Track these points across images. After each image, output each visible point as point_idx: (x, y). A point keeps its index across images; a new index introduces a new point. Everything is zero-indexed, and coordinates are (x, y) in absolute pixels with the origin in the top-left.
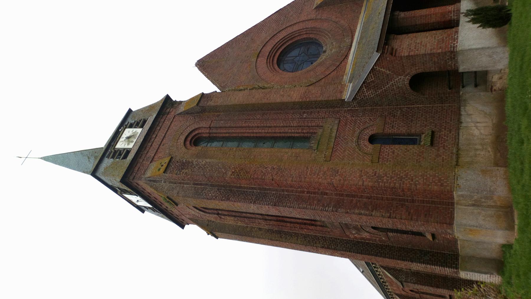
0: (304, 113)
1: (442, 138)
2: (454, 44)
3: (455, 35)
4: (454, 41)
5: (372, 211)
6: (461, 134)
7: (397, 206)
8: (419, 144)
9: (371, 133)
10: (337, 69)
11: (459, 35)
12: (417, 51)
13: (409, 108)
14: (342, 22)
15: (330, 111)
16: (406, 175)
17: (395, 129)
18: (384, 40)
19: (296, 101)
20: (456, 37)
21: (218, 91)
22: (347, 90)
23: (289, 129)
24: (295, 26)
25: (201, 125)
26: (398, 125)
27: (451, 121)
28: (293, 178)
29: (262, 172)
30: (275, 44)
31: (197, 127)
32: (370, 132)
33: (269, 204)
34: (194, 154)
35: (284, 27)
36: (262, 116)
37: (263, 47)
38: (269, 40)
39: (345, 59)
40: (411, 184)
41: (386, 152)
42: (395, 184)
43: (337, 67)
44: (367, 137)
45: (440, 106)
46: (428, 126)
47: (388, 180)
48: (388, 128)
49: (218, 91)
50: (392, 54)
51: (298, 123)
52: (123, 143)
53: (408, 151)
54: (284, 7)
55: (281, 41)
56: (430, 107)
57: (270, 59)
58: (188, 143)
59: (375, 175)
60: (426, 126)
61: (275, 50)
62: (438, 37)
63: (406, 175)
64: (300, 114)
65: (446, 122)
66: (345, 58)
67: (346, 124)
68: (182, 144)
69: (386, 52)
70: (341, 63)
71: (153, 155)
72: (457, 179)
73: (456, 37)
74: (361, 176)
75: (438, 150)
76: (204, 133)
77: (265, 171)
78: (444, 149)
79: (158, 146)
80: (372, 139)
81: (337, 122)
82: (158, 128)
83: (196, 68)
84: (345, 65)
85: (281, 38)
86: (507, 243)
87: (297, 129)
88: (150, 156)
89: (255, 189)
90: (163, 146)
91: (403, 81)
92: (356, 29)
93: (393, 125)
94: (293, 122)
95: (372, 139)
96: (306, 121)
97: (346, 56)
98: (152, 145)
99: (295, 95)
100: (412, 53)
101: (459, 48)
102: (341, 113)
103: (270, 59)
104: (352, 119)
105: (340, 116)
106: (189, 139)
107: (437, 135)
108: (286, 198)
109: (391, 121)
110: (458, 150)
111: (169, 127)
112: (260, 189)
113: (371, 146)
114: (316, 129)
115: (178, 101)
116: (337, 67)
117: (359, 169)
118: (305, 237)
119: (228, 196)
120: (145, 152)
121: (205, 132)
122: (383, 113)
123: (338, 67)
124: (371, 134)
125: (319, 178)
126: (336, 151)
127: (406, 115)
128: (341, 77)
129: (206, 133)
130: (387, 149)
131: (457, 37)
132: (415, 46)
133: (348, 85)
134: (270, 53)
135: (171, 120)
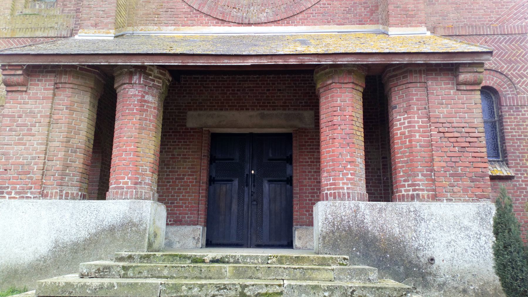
2: (9, 193)
3: (32, 193)
4: (16, 193)
10: (195, 11)
11: (32, 200)
12: (11, 130)
18: (28, 64)
20: (29, 195)
22: (96, 35)
43: (198, 11)
66: (218, 19)
70: (207, 15)
86: (64, 276)
97: (222, 20)
116: (198, 11)
118: (349, 67)
123: (198, 12)
128: (172, 22)
132: (25, 125)
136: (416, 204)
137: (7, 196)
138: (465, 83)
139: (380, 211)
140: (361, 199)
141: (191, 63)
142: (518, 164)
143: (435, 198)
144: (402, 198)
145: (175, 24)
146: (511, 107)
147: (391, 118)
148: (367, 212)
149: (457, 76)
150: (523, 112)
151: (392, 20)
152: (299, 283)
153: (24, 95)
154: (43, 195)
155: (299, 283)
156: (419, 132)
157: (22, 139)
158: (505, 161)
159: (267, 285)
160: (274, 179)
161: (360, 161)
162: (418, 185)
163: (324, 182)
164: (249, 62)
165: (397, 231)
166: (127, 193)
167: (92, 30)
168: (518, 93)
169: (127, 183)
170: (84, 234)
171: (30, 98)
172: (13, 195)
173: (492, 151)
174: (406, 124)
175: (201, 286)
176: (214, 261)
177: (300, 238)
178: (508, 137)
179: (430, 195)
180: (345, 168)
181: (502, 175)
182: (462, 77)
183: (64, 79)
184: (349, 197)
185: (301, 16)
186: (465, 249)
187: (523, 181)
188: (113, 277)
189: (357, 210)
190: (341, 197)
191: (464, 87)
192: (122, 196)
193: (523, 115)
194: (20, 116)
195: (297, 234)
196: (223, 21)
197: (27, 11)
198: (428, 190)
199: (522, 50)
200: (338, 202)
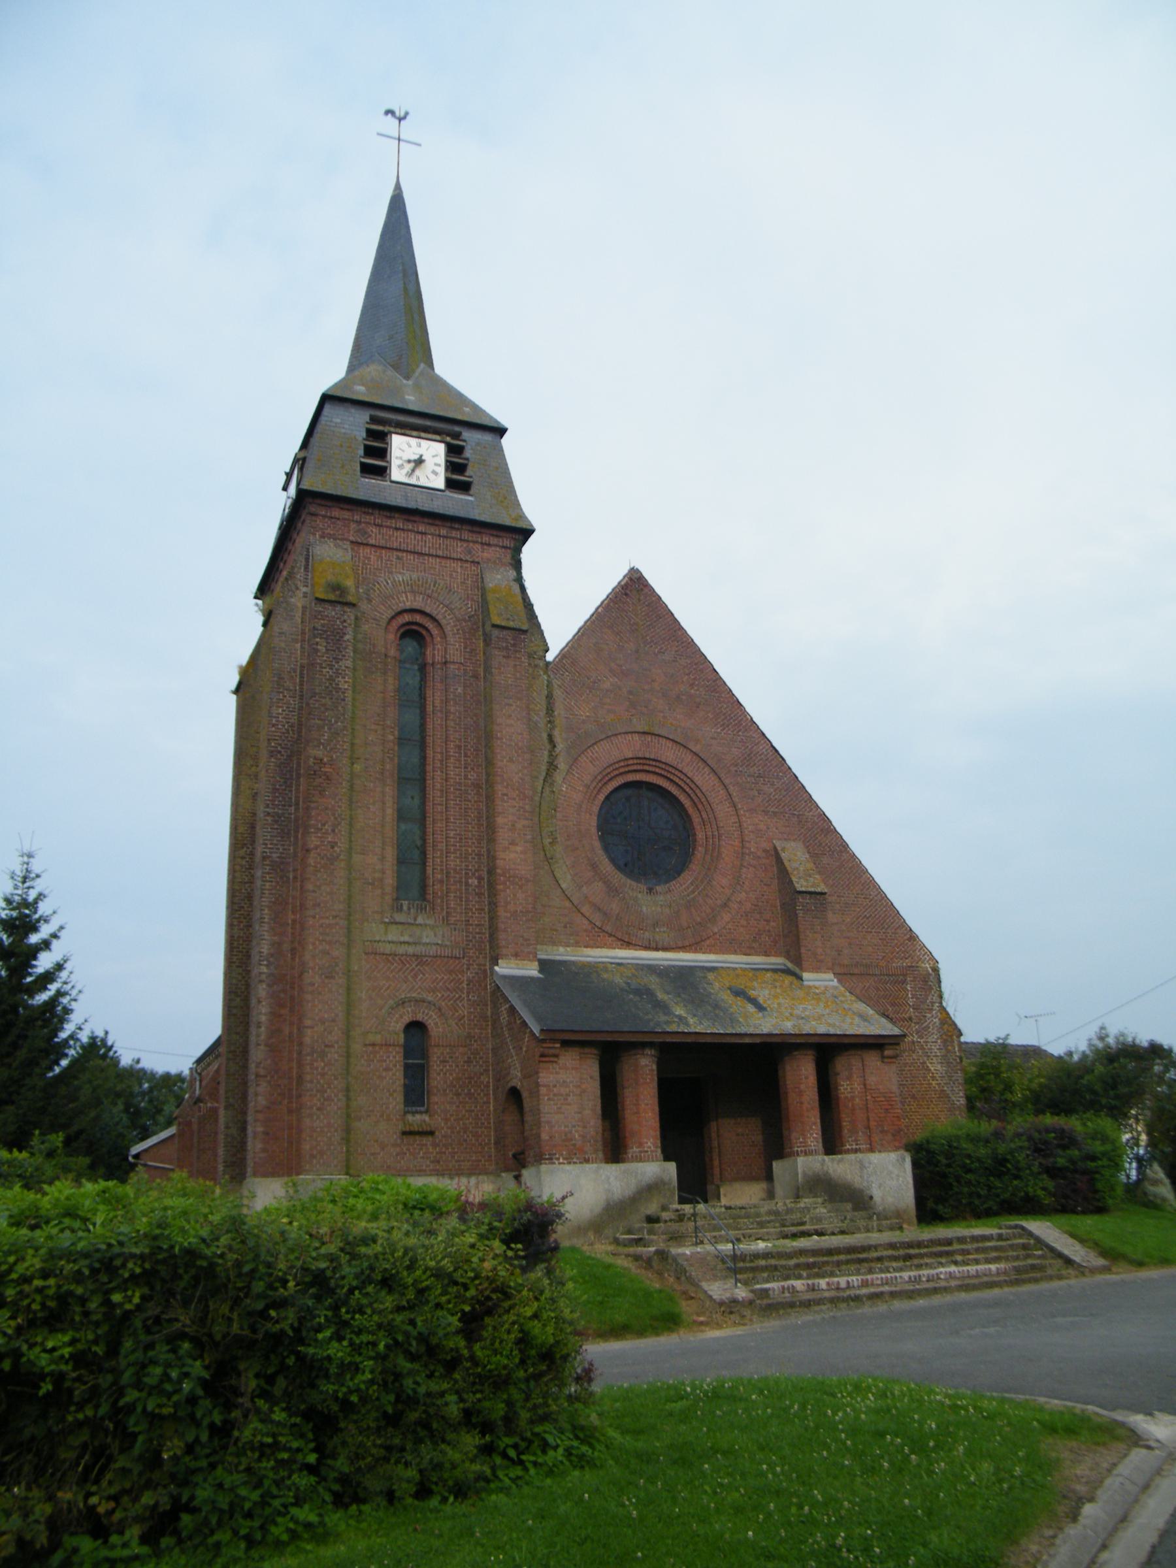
0: (480, 879)
1: (421, 1149)
3: (578, 1158)
4: (564, 1159)
5: (266, 1045)
7: (279, 1086)
8: (406, 1113)
9: (430, 1024)
12: (549, 1099)
13: (487, 1086)
14: (726, 917)
15: (484, 934)
16: (329, 1099)
17: (438, 1066)
19: (498, 861)
20: (575, 1160)
23: (442, 850)
25: (451, 639)
26: (447, 1070)
27: (457, 1161)
28: (314, 891)
29: (324, 825)
30: (680, 767)
31: (448, 629)
32: (432, 1020)
33: (266, 844)
34: (374, 646)
35: (727, 782)
36: (473, 784)
37: (673, 740)
38: (692, 751)
39: (619, 943)
40: (311, 1108)
42: (311, 1082)
45: (490, 1140)
46: (446, 1124)
47: (317, 1068)
48: (442, 1053)
49: (550, 657)
50: (542, 1055)
51: (455, 870)
53: (391, 1095)
54: (790, 768)
55: (688, 781)
56: (489, 1123)
58: (407, 618)
59: (326, 1046)
60: (446, 1120)
61: (663, 772)
62: (576, 1131)
63: (329, 1099)
64: (476, 871)
65: (455, 1153)
67: (451, 972)
68: (401, 606)
69: (545, 1045)
70: (610, 935)
71: (372, 542)
74: (322, 1021)
75: (395, 1145)
76: (434, 649)
77: (327, 830)
78: (397, 1155)
79: (395, 545)
80: (416, 1028)
81: (456, 953)
82: (443, 532)
83: (625, 571)
84: (605, 944)
85: (696, 779)
87: (442, 870)
88: (370, 536)
89: (297, 809)
90: (398, 558)
91: (516, 1079)
92: (704, 953)
93: (448, 1062)
94: (457, 857)
95: (416, 1028)
96: (461, 886)
98: (397, 529)
99: (512, 855)
100: (543, 1090)
101: (544, 1168)
102: (478, 957)
104: (463, 982)
105: (470, 957)
106: (418, 618)
107: (427, 1140)
108: (281, 878)
109: (457, 1058)
111: (446, 558)
112: (296, 820)
113: (400, 1026)
114: (442, 909)
115: (522, 555)
117: (337, 1015)
119: (280, 752)
120: (378, 521)
121: (434, 653)
122: (475, 1041)
124: (427, 1023)
125: (314, 944)
126: (388, 961)
127: (470, 1082)
129: (434, 655)
130: (395, 1057)
131: (575, 1163)
134: (654, 760)
135: (468, 558)
136: (860, 1155)
144: (848, 1152)
147: (1029, 1217)
149: (882, 1052)
151: (805, 964)
153: (554, 1065)
157: (560, 1108)
167: (513, 962)
171: (560, 1068)
172: (561, 1161)
177: (725, 1195)
179: (814, 1137)
180: (811, 1129)
182: (887, 1053)
183: (587, 1050)
186: (692, 1298)
194: (555, 1086)
196: (628, 944)
200: (810, 1158)
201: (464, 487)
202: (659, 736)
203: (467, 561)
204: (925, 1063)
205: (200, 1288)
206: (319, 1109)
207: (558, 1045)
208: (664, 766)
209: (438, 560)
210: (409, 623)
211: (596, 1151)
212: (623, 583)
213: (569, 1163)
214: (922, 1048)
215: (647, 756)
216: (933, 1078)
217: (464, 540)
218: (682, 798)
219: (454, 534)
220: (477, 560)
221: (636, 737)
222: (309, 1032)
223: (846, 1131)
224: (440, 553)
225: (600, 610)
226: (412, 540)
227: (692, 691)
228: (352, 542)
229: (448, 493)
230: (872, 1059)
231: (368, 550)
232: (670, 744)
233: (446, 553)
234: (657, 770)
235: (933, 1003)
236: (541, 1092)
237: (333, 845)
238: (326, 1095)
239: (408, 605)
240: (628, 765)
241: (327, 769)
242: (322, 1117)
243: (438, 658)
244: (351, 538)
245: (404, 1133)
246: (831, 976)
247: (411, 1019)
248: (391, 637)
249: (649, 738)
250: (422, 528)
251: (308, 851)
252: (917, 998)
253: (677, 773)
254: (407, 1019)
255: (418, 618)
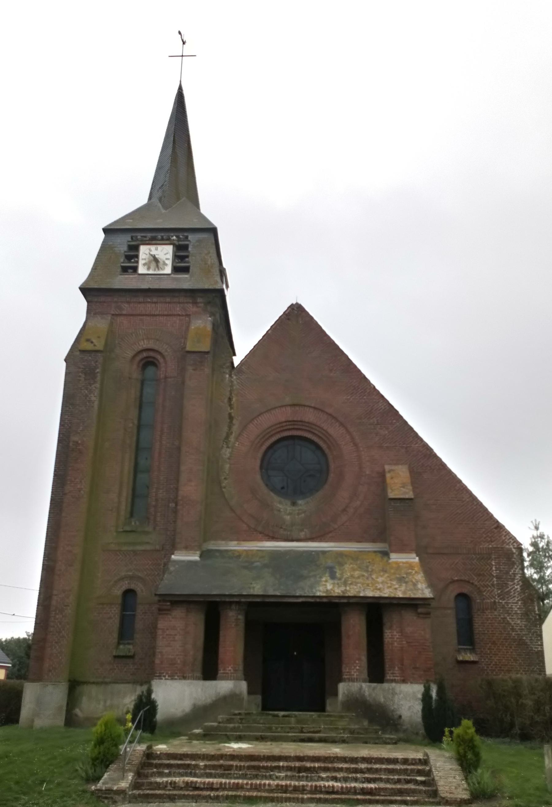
2: (165, 676)
3: (178, 676)
6: (127, 685)
21: (237, 361)
24: (352, 447)
41: (111, 611)
42: (54, 627)
44: (132, 586)
49: (237, 361)
52: (147, 254)
57: (289, 425)
58: (145, 354)
62: (179, 658)
68: (140, 348)
69: (161, 604)
70: (261, 533)
72: (54, 684)
73: (176, 677)
81: (158, 547)
82: (168, 300)
95: (129, 593)
98: (140, 303)
100: (159, 632)
103: (289, 425)
106: (151, 354)
110: (106, 683)
111: (170, 315)
131: (176, 679)
133: (196, 554)
136: (394, 685)
137: (164, 678)
138: (421, 613)
139: (374, 689)
140: (364, 681)
141: (267, 600)
142: (482, 652)
143: (404, 681)
145: (238, 540)
146: (479, 610)
148: (367, 689)
150: (487, 614)
152: (329, 726)
153: (169, 616)
154: (184, 678)
155: (329, 726)
156: (396, 641)
158: (473, 650)
159: (313, 727)
160: (163, 276)
161: (364, 659)
162: (395, 673)
163: (344, 670)
164: (300, 600)
165: (382, 700)
166: (231, 676)
168: (484, 599)
169: (230, 670)
170: (209, 701)
172: (167, 677)
173: (107, 789)
174: (390, 636)
175: (282, 727)
176: (284, 716)
178: (476, 631)
180: (355, 662)
181: (469, 660)
182: (420, 610)
184: (357, 680)
185: (330, 535)
187: (485, 664)
188: (234, 723)
189: (361, 688)
190: (353, 680)
191: (421, 616)
192: (226, 678)
193: (487, 615)
194: (167, 629)
195: (328, 702)
197: (127, 528)
198: (400, 677)
199: (488, 566)
200: (351, 684)
201: (186, 270)
202: (305, 406)
203: (182, 315)
204: (505, 618)
205: (129, 736)
206: (56, 643)
207: (169, 604)
208: (307, 425)
209: (165, 317)
210: (147, 357)
211: (236, 671)
212: (287, 312)
213: (172, 679)
214: (503, 607)
215: (295, 419)
216: (513, 629)
217: (182, 303)
218: (321, 443)
219: (176, 300)
220: (188, 313)
221: (289, 409)
222: (55, 598)
223: (387, 666)
224: (166, 313)
225: (269, 332)
226: (149, 308)
227: (332, 374)
228: (113, 315)
229: (173, 276)
230: (409, 616)
231: (122, 318)
232: (311, 410)
233: (170, 313)
234: (303, 428)
235: (514, 574)
236: (158, 633)
237: (80, 489)
238: (61, 634)
239: (145, 346)
240: (282, 427)
241: (80, 447)
242: (57, 647)
243: (162, 376)
244: (112, 312)
245: (115, 657)
246: (414, 555)
247: (127, 588)
248: (135, 366)
249: (297, 408)
250: (155, 300)
251: (65, 494)
252: (500, 571)
253: (316, 428)
254: (124, 588)
255: (151, 354)
